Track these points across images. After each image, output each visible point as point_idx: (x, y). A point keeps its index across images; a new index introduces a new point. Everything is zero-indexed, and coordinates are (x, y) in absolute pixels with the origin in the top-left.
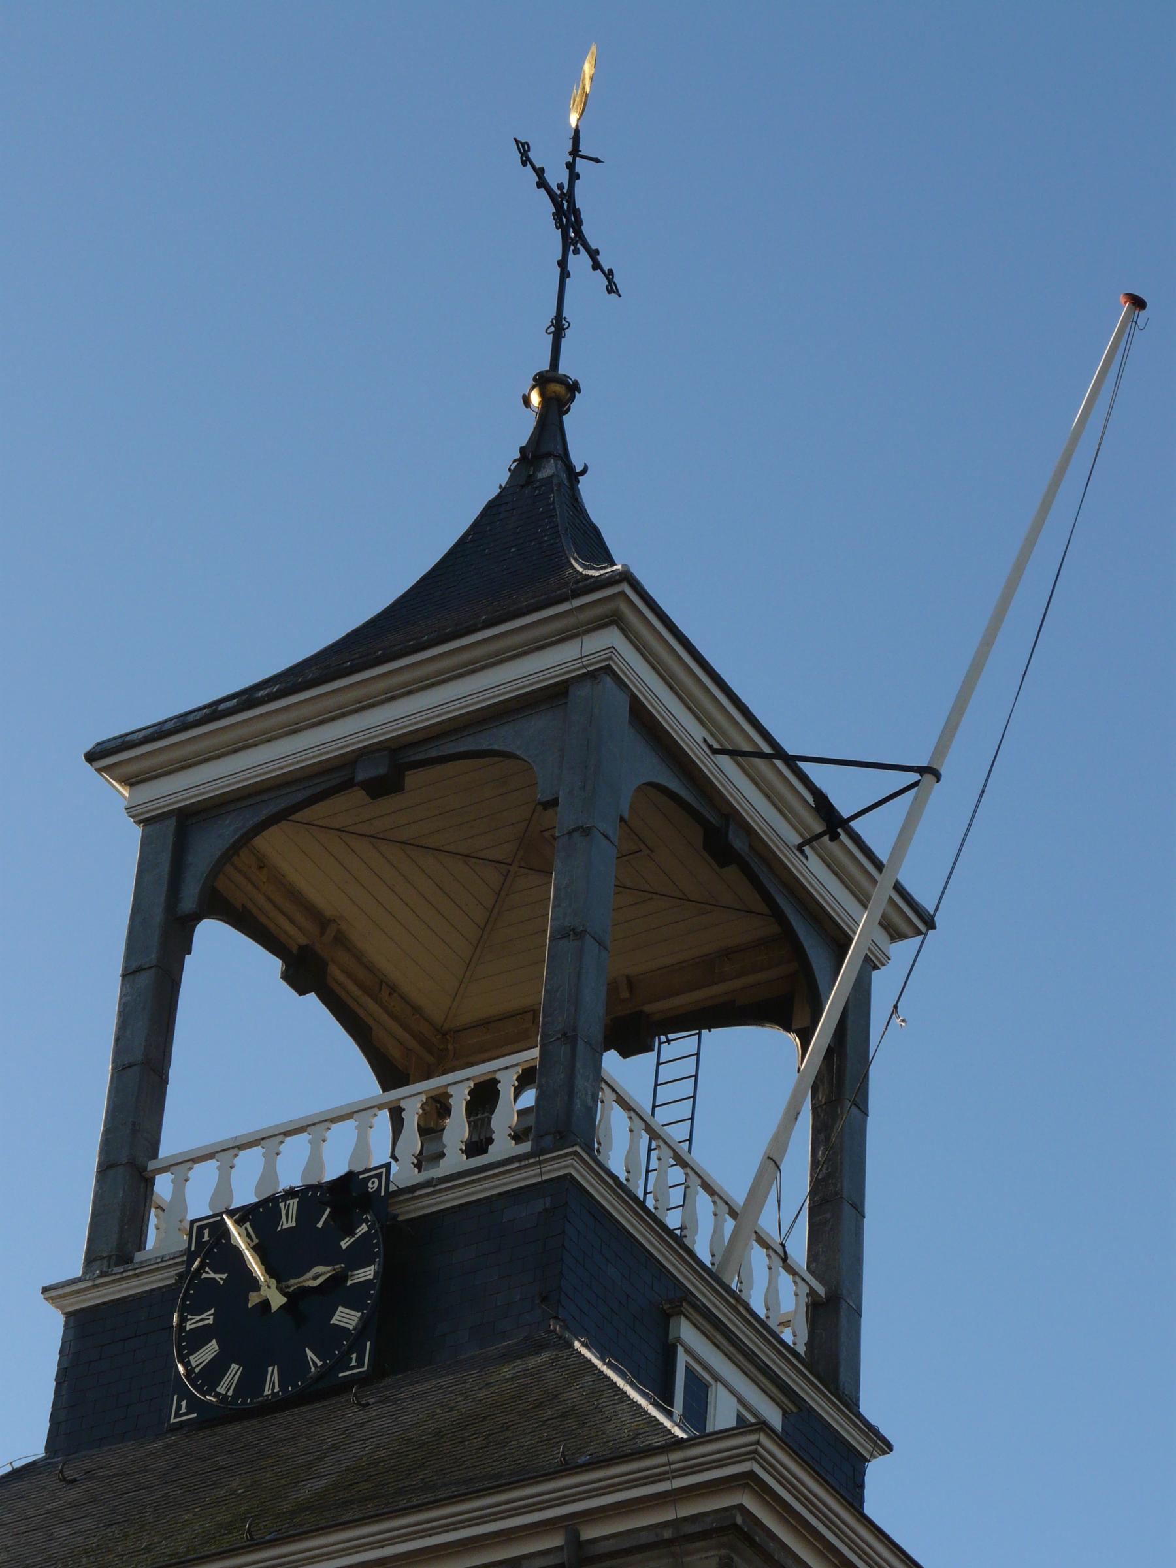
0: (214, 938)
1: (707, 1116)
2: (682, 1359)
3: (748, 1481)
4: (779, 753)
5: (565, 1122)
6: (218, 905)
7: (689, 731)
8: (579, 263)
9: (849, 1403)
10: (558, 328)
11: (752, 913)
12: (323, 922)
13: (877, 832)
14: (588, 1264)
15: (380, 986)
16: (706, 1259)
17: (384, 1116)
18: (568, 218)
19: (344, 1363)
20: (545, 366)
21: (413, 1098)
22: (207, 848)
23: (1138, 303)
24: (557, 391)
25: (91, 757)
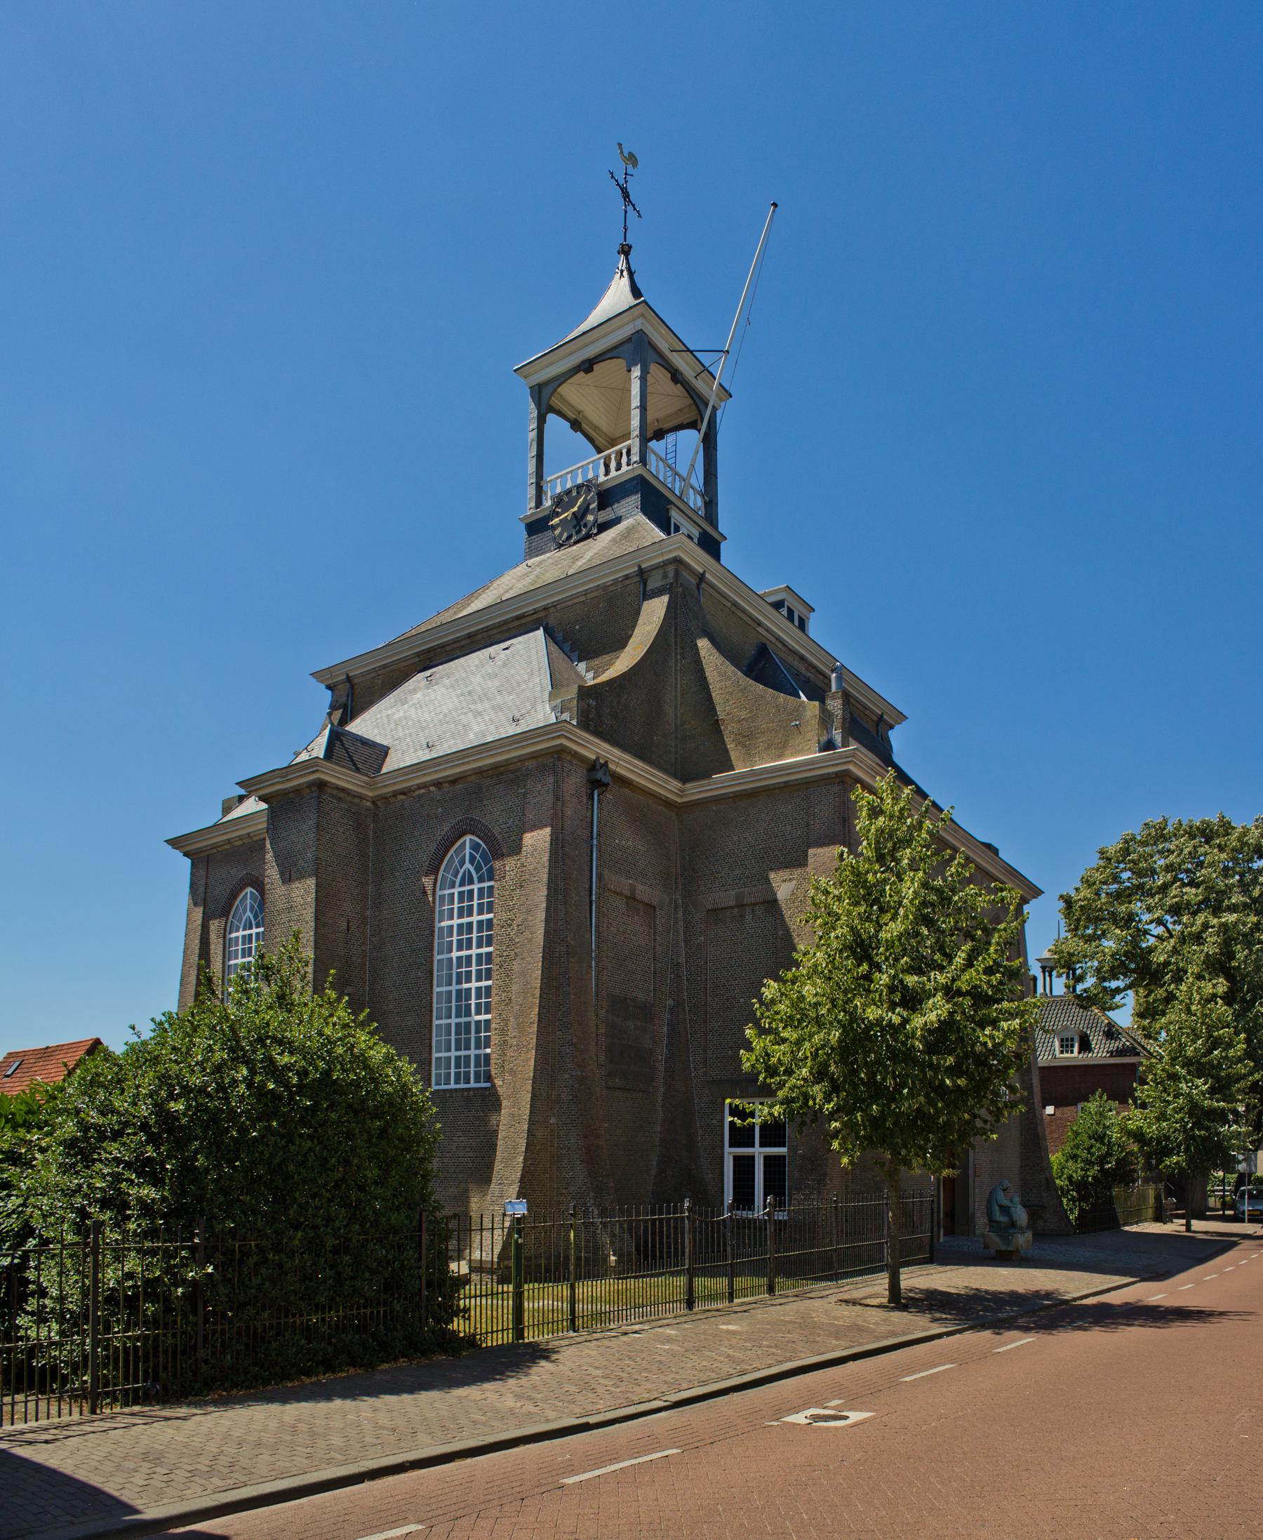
4: (688, 350)
9: (715, 527)
15: (596, 428)
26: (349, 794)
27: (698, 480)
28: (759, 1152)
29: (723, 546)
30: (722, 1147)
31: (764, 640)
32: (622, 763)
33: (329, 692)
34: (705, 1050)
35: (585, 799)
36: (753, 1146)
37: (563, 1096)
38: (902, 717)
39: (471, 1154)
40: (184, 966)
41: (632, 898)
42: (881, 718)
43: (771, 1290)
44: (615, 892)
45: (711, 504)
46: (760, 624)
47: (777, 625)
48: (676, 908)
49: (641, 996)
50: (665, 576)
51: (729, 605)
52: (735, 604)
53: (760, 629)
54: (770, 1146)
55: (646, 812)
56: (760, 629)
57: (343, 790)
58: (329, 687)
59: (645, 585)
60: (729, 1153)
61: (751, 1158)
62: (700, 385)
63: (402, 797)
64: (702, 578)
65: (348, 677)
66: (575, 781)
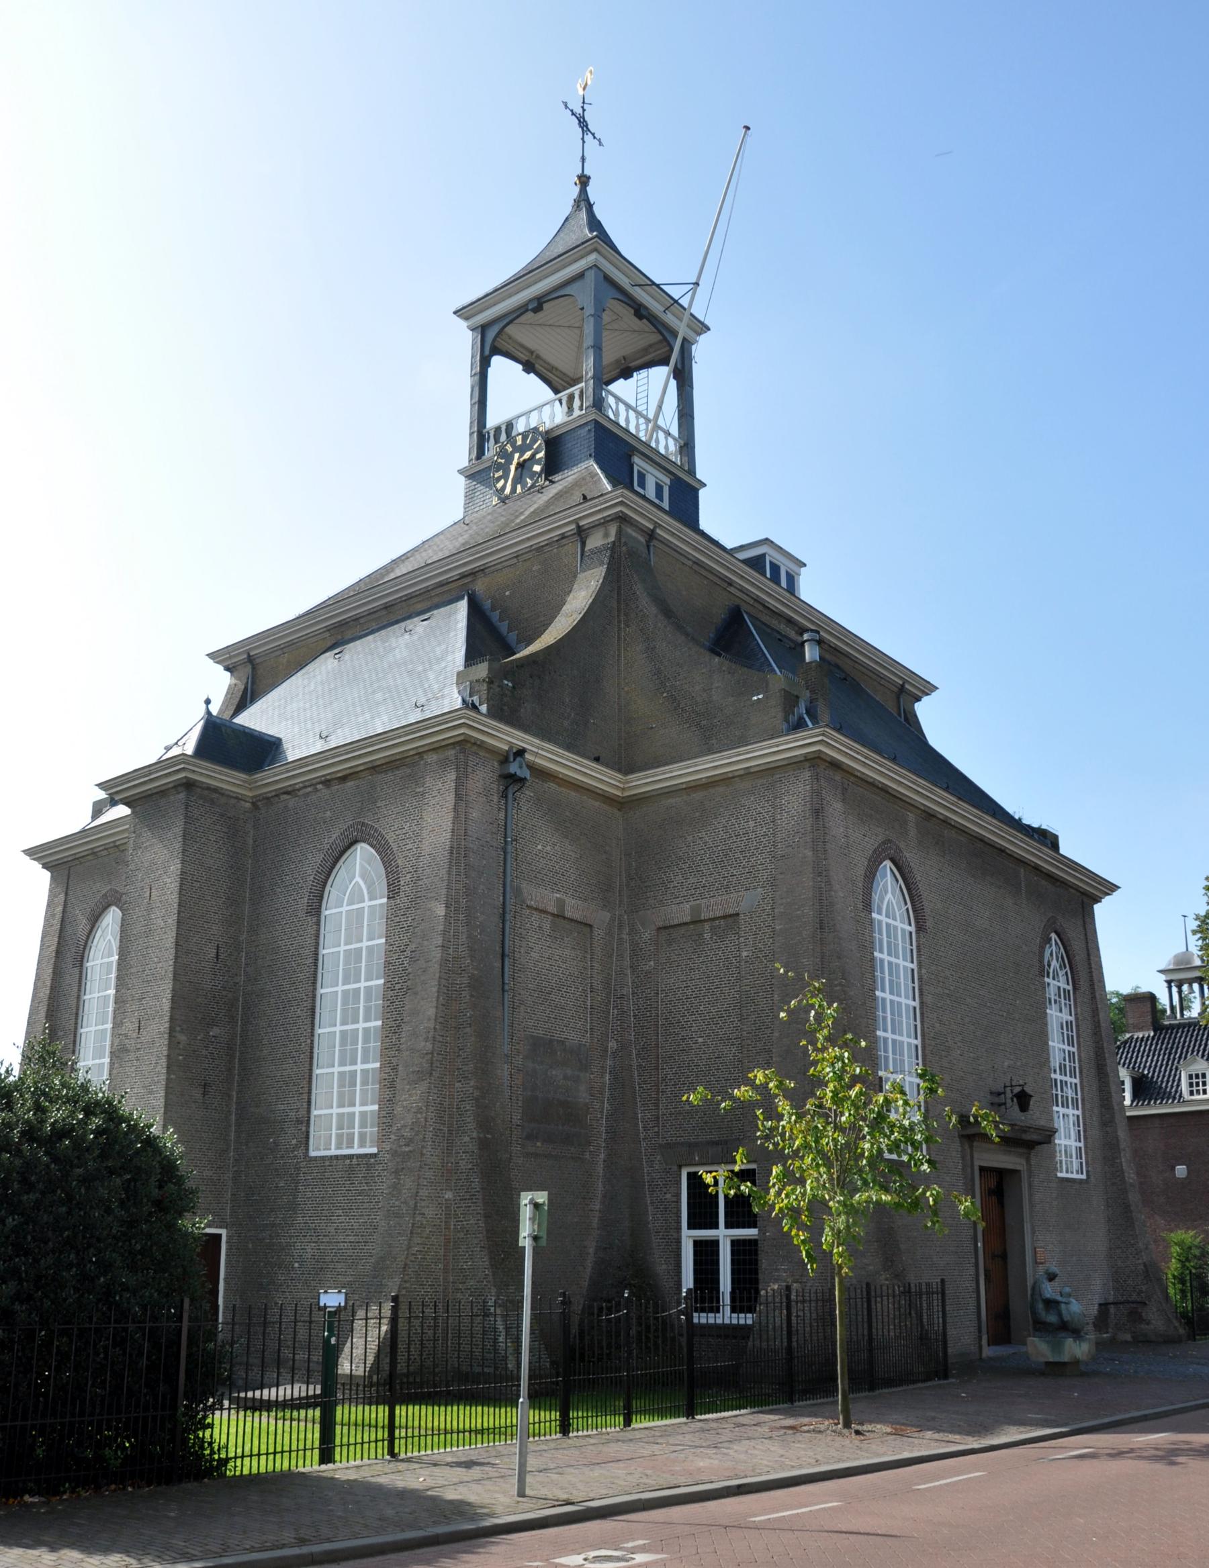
0: (497, 361)
1: (642, 399)
2: (636, 468)
3: (621, 503)
4: (654, 283)
5: (599, 404)
6: (496, 351)
7: (623, 281)
8: (588, 137)
9: (692, 472)
10: (583, 159)
11: (656, 333)
12: (532, 352)
13: (684, 302)
14: (617, 451)
15: (552, 369)
16: (644, 439)
17: (557, 403)
18: (583, 124)
19: (537, 481)
20: (580, 172)
21: (564, 395)
22: (491, 334)
23: (747, 128)
24: (584, 181)
25: (455, 313)
26: (223, 794)
27: (670, 419)
28: (724, 1235)
29: (702, 493)
30: (679, 1229)
31: (738, 602)
32: (544, 753)
33: (228, 674)
34: (657, 1105)
35: (495, 798)
36: (717, 1227)
37: (462, 1164)
38: (1111, 888)
39: (352, 1239)
40: (33, 1000)
41: (560, 916)
42: (902, 689)
43: (565, 1428)
44: (536, 909)
45: (687, 445)
46: (731, 583)
47: (756, 585)
48: (620, 926)
49: (573, 1037)
50: (606, 535)
51: (690, 563)
52: (697, 563)
53: (732, 589)
54: (700, 1228)
55: (570, 810)
56: (732, 589)
57: (216, 790)
58: (227, 669)
59: (583, 544)
60: (688, 1237)
61: (714, 1244)
62: (669, 319)
63: (286, 797)
64: (651, 535)
65: (249, 656)
66: (483, 777)
